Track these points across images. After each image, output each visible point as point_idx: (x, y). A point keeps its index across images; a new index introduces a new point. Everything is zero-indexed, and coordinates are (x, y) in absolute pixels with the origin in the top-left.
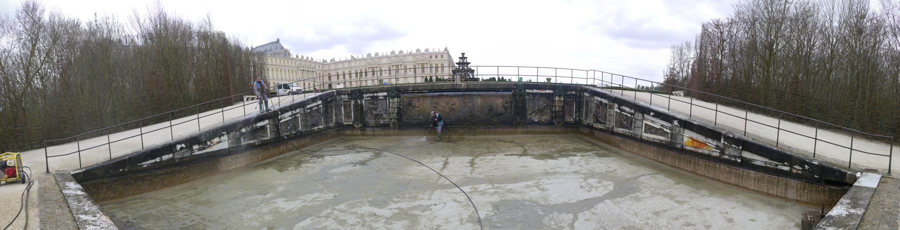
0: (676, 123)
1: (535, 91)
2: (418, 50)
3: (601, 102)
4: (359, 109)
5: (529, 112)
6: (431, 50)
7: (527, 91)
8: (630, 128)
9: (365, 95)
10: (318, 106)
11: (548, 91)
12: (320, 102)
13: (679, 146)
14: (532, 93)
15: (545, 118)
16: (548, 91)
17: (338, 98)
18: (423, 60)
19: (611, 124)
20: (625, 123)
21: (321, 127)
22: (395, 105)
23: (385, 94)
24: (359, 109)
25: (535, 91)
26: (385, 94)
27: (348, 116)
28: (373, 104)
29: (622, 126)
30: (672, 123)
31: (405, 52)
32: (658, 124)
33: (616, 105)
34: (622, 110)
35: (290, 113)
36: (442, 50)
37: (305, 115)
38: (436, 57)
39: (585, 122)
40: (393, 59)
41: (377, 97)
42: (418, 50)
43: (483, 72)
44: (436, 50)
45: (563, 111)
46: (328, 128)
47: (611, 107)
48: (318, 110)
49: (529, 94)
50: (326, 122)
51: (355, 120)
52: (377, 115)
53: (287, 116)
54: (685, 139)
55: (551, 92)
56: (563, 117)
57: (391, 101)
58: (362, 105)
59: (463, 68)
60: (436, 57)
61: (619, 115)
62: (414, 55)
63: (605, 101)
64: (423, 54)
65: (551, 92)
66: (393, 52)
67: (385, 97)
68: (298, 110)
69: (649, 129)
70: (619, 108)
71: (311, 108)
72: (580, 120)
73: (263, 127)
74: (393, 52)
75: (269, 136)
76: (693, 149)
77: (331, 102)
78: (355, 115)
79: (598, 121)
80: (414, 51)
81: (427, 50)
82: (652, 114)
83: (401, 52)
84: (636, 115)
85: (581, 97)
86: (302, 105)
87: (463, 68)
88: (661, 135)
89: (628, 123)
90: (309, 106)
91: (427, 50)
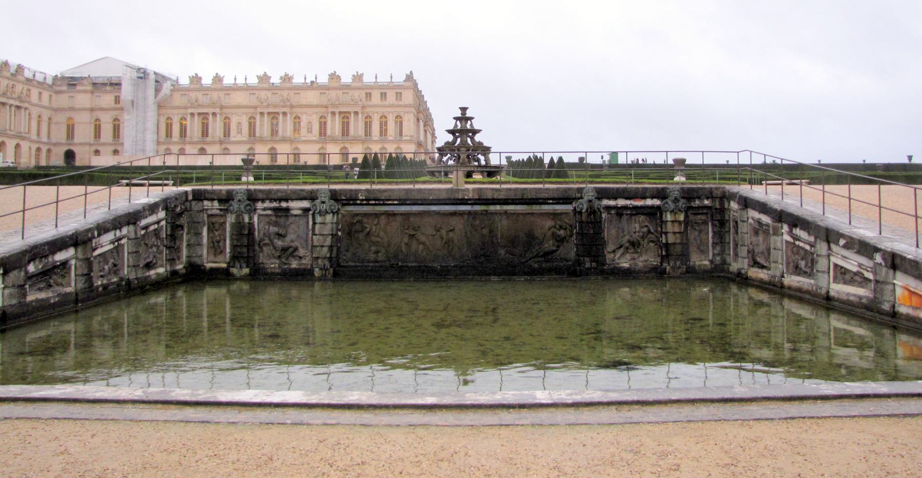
0: (878, 258)
1: (621, 202)
2: (334, 76)
3: (759, 222)
4: (244, 233)
5: (610, 247)
6: (368, 79)
7: (606, 202)
8: (809, 275)
9: (260, 205)
10: (158, 222)
11: (649, 202)
12: (162, 214)
13: (886, 307)
14: (615, 207)
15: (648, 258)
16: (649, 202)
17: (196, 206)
18: (345, 101)
19: (777, 269)
20: (802, 264)
21: (161, 270)
22: (327, 230)
23: (305, 204)
24: (244, 233)
25: (621, 202)
26: (305, 204)
27: (216, 247)
28: (276, 224)
29: (797, 270)
30: (871, 258)
31: (298, 80)
32: (852, 262)
33: (786, 228)
34: (796, 238)
35: (110, 236)
36: (399, 78)
37: (137, 241)
38: (383, 96)
39: (734, 267)
40: (263, 94)
41: (287, 210)
42: (334, 76)
43: (508, 139)
44: (384, 79)
45: (685, 245)
46: (174, 273)
47: (776, 232)
48: (156, 233)
49: (608, 208)
50: (172, 261)
51: (235, 258)
52: (285, 250)
53: (105, 243)
54: (899, 292)
55: (656, 202)
56: (684, 256)
57: (319, 219)
58: (251, 225)
59: (464, 143)
60: (383, 96)
61: (793, 247)
62: (323, 88)
63: (765, 219)
64: (347, 87)
65: (656, 202)
66: (264, 78)
67: (306, 210)
68: (125, 230)
69: (842, 274)
70: (790, 233)
71: (146, 228)
72: (724, 262)
73: (65, 264)
74: (264, 78)
75: (72, 285)
76: (910, 311)
77: (180, 215)
78: (234, 247)
79: (756, 264)
80: (323, 79)
81: (358, 77)
82: (842, 242)
83: (287, 78)
84: (818, 246)
85: (722, 210)
86: (132, 218)
87: (464, 143)
88: (860, 285)
89: (804, 262)
90: (143, 222)
91: (358, 77)
